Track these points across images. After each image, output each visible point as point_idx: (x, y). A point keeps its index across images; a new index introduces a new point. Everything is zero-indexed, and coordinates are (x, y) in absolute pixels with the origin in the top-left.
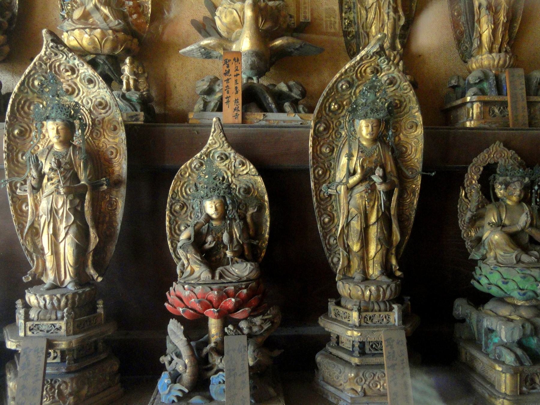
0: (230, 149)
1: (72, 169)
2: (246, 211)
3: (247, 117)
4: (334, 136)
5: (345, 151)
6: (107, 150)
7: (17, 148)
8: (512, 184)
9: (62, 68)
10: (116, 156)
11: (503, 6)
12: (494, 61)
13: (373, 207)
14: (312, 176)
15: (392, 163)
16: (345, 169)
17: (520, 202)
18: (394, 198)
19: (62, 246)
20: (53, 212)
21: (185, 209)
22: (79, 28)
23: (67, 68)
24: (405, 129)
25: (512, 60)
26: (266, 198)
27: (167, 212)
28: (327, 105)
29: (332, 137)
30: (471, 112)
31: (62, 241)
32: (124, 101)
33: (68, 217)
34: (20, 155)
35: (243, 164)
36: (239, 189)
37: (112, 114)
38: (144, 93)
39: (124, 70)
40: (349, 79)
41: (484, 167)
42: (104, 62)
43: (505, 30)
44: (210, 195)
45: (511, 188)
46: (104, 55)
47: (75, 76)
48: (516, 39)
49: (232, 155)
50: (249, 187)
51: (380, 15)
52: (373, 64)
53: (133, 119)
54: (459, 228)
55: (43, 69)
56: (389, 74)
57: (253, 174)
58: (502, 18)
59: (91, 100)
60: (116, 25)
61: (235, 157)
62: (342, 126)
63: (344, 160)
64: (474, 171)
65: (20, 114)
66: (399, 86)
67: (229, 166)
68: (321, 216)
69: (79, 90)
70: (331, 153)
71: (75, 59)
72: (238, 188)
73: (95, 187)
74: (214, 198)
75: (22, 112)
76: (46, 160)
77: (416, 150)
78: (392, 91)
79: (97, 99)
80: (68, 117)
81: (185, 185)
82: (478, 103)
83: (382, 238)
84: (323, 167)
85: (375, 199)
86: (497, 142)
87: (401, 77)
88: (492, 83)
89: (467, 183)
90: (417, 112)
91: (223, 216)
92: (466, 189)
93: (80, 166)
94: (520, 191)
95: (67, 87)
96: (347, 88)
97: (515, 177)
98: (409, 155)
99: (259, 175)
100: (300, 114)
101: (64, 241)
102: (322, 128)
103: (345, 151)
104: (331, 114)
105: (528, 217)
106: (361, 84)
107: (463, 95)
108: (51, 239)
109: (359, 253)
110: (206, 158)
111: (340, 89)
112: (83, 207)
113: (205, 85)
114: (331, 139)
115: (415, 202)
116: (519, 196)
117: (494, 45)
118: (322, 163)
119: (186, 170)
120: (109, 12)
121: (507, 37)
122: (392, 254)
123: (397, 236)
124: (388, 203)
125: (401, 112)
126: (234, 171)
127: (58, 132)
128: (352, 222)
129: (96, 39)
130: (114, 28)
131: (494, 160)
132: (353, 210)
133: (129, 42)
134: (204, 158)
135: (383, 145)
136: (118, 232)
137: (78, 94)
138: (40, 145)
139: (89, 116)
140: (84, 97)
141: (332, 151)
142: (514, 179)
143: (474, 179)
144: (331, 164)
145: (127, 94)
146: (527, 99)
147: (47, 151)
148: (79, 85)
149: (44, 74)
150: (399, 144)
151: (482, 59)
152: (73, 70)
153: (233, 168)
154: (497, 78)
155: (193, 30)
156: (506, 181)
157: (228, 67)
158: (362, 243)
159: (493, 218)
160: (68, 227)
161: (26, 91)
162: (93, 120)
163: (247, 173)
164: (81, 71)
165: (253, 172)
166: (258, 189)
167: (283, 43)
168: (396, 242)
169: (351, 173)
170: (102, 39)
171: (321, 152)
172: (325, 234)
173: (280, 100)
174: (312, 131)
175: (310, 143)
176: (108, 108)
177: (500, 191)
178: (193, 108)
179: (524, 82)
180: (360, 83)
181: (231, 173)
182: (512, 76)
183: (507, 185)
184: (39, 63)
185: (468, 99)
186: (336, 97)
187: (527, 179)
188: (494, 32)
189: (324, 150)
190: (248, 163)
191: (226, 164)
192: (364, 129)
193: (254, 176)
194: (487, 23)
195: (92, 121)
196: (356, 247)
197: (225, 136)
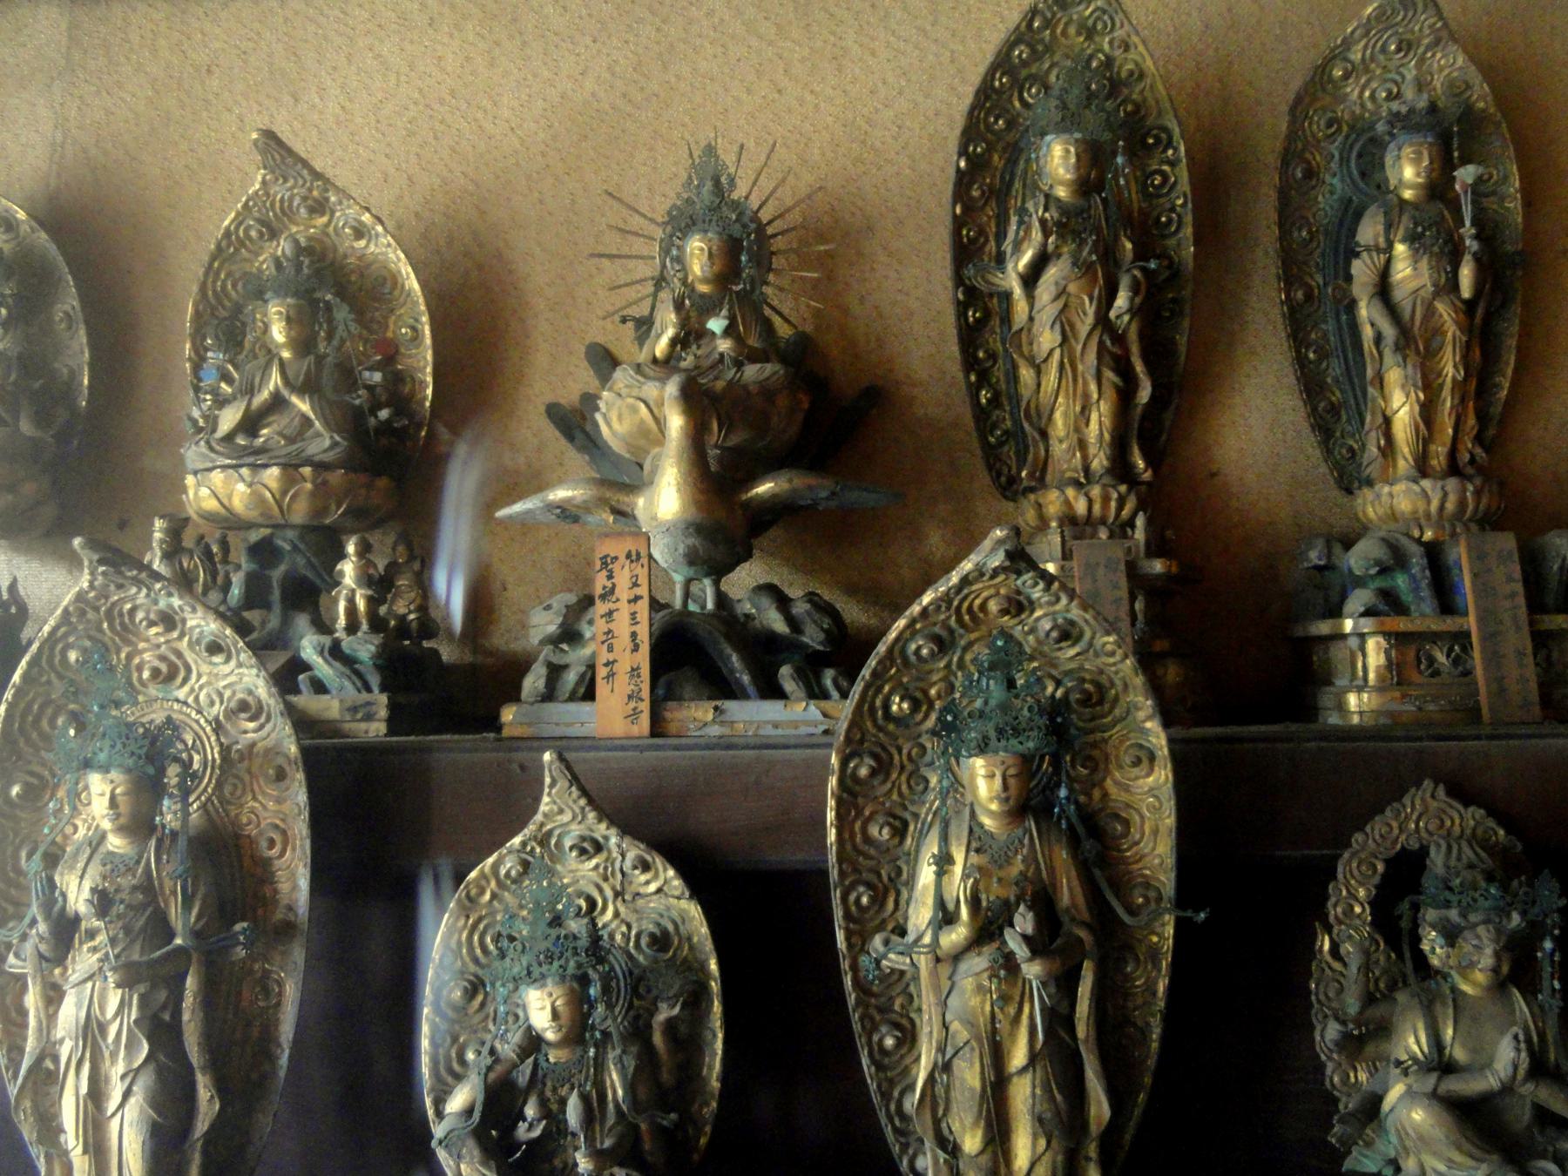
0: (603, 826)
1: (149, 904)
2: (652, 1012)
3: (668, 715)
4: (904, 787)
5: (932, 847)
6: (261, 834)
7: (16, 835)
8: (1467, 934)
9: (140, 615)
10: (282, 854)
11: (1450, 334)
12: (1429, 502)
13: (1016, 1020)
14: (838, 914)
15: (1076, 883)
16: (930, 901)
17: (1500, 985)
18: (1085, 989)
19: (114, 1125)
20: (91, 1030)
21: (480, 998)
22: (224, 467)
23: (152, 616)
24: (1120, 767)
25: (1484, 501)
26: (713, 966)
27: (426, 1011)
28: (878, 702)
29: (900, 794)
30: (1360, 665)
31: (114, 1115)
32: (337, 664)
33: (131, 1046)
34: (23, 854)
35: (645, 866)
36: (638, 936)
37: (273, 735)
38: (412, 617)
39: (342, 573)
40: (937, 629)
41: (1387, 862)
42: (295, 547)
43: (1463, 400)
44: (536, 971)
45: (1466, 945)
46: (293, 527)
47: (175, 634)
48: (1503, 422)
49: (613, 840)
50: (665, 933)
51: (1075, 380)
52: (1002, 591)
53: (359, 716)
54: (1318, 1056)
55: (89, 621)
56: (1054, 613)
57: (677, 893)
58: (1449, 370)
59: (221, 695)
60: (325, 451)
61: (624, 850)
62: (927, 758)
63: (926, 874)
64: (1356, 872)
65: (28, 740)
66: (1091, 644)
67: (606, 868)
68: (871, 1028)
69: (189, 670)
70: (896, 840)
71: (170, 595)
72: (633, 933)
73: (211, 947)
74: (549, 981)
75: (34, 735)
76: (82, 877)
77: (1155, 832)
78: (1072, 658)
79: (234, 693)
80: (141, 762)
81: (481, 926)
82: (1381, 639)
83: (1048, 1115)
84: (876, 881)
85: (1023, 994)
86: (1427, 784)
87: (1092, 621)
88: (1419, 576)
89: (1335, 911)
90: (1149, 718)
91: (578, 1030)
92: (1335, 931)
93: (174, 893)
94: (1497, 955)
95: (157, 663)
96: (932, 654)
97: (1476, 910)
98: (1137, 843)
99: (691, 897)
100: (823, 704)
101: (119, 1115)
102: (863, 772)
103: (932, 847)
104: (891, 727)
105: (1518, 1050)
106: (977, 640)
107: (1336, 612)
108: (85, 1106)
109: (985, 1160)
110: (538, 850)
111: (913, 658)
112: (177, 1013)
113: (551, 622)
114: (895, 797)
115: (1161, 987)
116: (1496, 970)
117: (1433, 448)
118: (871, 870)
119: (483, 883)
120: (313, 408)
121: (1471, 421)
122: (1088, 1159)
123: (1100, 1107)
124: (1065, 1004)
125: (1103, 716)
126: (622, 883)
127: (113, 803)
128: (956, 1062)
129: (268, 495)
130: (317, 458)
131: (1420, 839)
132: (960, 1032)
133: (363, 491)
134: (533, 849)
135: (1044, 826)
136: (282, 1073)
137: (185, 680)
138: (79, 823)
139: (213, 739)
140: (201, 688)
141: (900, 832)
142: (1473, 918)
143: (1357, 899)
144: (899, 871)
145: (348, 643)
146: (1531, 623)
147: (88, 851)
148: (190, 657)
149: (92, 633)
150: (1102, 810)
151: (1391, 495)
152: (169, 621)
153: (619, 876)
154: (1433, 552)
155: (551, 433)
156: (1448, 920)
157: (610, 577)
158: (989, 1126)
159: (1413, 1042)
160: (132, 1075)
161: (44, 679)
162: (225, 751)
163: (659, 891)
164: (190, 624)
165: (676, 888)
166: (689, 939)
167: (777, 490)
168: (1099, 1124)
169: (945, 917)
170: (284, 493)
171: (868, 839)
172: (885, 1085)
173: (766, 662)
174: (833, 782)
175: (830, 816)
176: (262, 720)
177: (1433, 944)
178: (518, 688)
179: (1518, 574)
180: (973, 636)
181: (613, 888)
182: (1479, 556)
183: (1451, 936)
184: (77, 609)
185: (1348, 625)
186: (905, 680)
187: (1516, 919)
188: (1427, 412)
189: (874, 831)
190: (659, 862)
191: (596, 867)
192: (983, 780)
193: (679, 898)
194: (1403, 387)
195: (220, 753)
196: (971, 1143)
197: (584, 792)
